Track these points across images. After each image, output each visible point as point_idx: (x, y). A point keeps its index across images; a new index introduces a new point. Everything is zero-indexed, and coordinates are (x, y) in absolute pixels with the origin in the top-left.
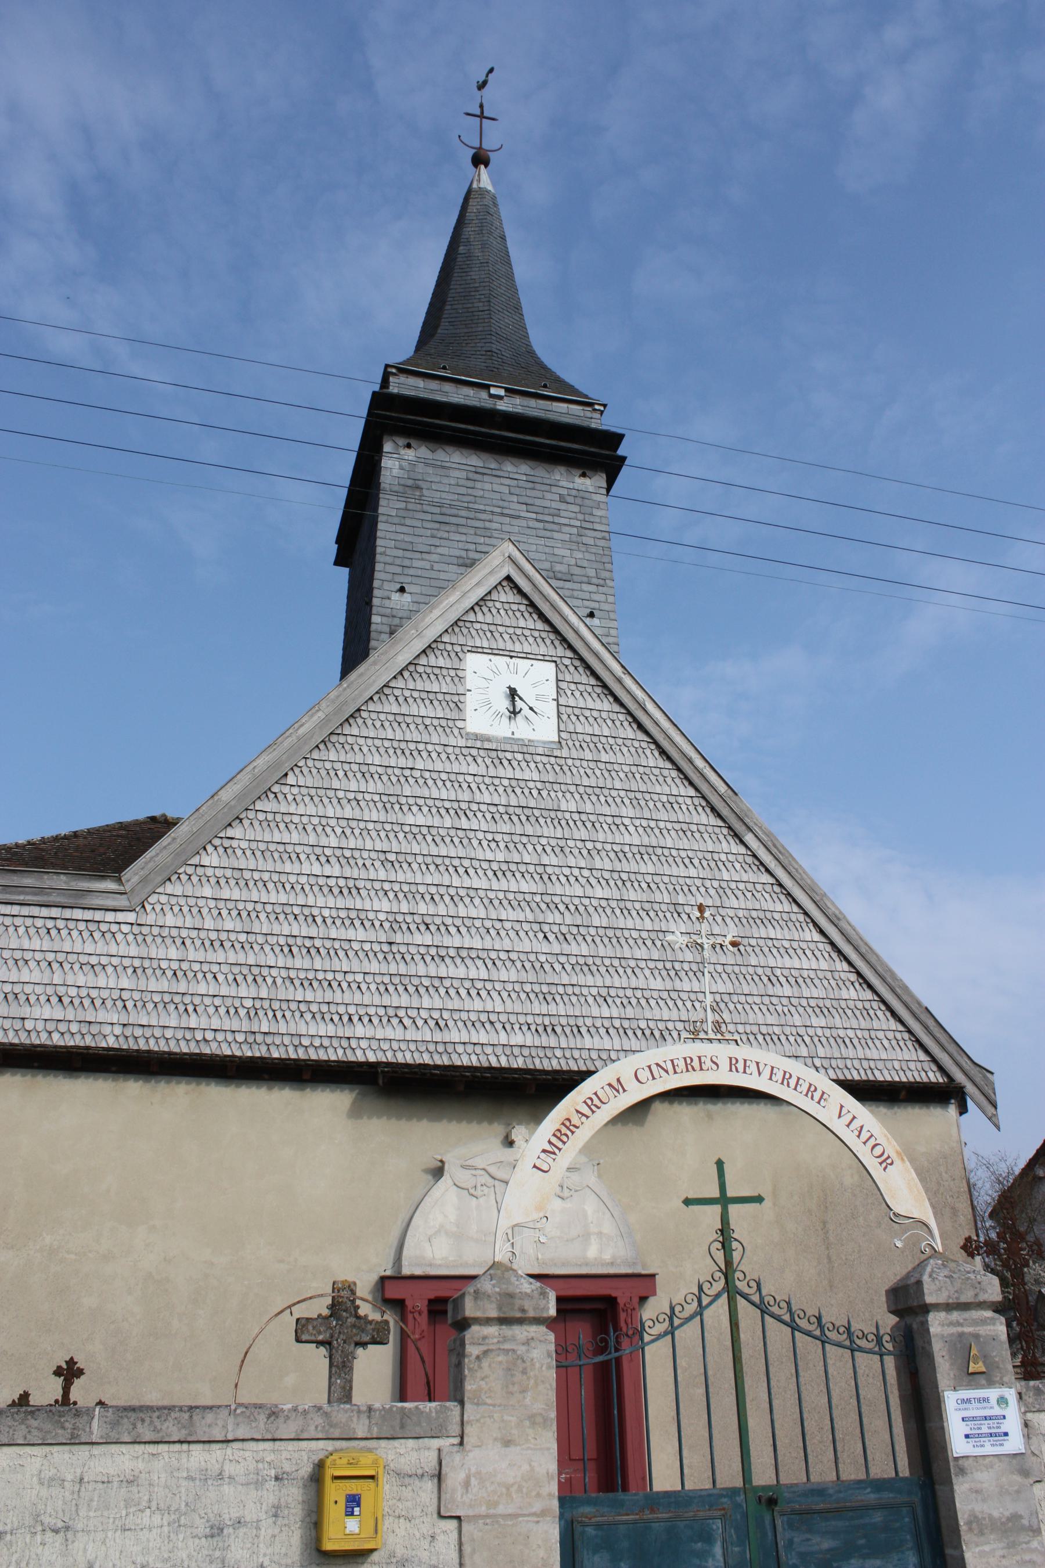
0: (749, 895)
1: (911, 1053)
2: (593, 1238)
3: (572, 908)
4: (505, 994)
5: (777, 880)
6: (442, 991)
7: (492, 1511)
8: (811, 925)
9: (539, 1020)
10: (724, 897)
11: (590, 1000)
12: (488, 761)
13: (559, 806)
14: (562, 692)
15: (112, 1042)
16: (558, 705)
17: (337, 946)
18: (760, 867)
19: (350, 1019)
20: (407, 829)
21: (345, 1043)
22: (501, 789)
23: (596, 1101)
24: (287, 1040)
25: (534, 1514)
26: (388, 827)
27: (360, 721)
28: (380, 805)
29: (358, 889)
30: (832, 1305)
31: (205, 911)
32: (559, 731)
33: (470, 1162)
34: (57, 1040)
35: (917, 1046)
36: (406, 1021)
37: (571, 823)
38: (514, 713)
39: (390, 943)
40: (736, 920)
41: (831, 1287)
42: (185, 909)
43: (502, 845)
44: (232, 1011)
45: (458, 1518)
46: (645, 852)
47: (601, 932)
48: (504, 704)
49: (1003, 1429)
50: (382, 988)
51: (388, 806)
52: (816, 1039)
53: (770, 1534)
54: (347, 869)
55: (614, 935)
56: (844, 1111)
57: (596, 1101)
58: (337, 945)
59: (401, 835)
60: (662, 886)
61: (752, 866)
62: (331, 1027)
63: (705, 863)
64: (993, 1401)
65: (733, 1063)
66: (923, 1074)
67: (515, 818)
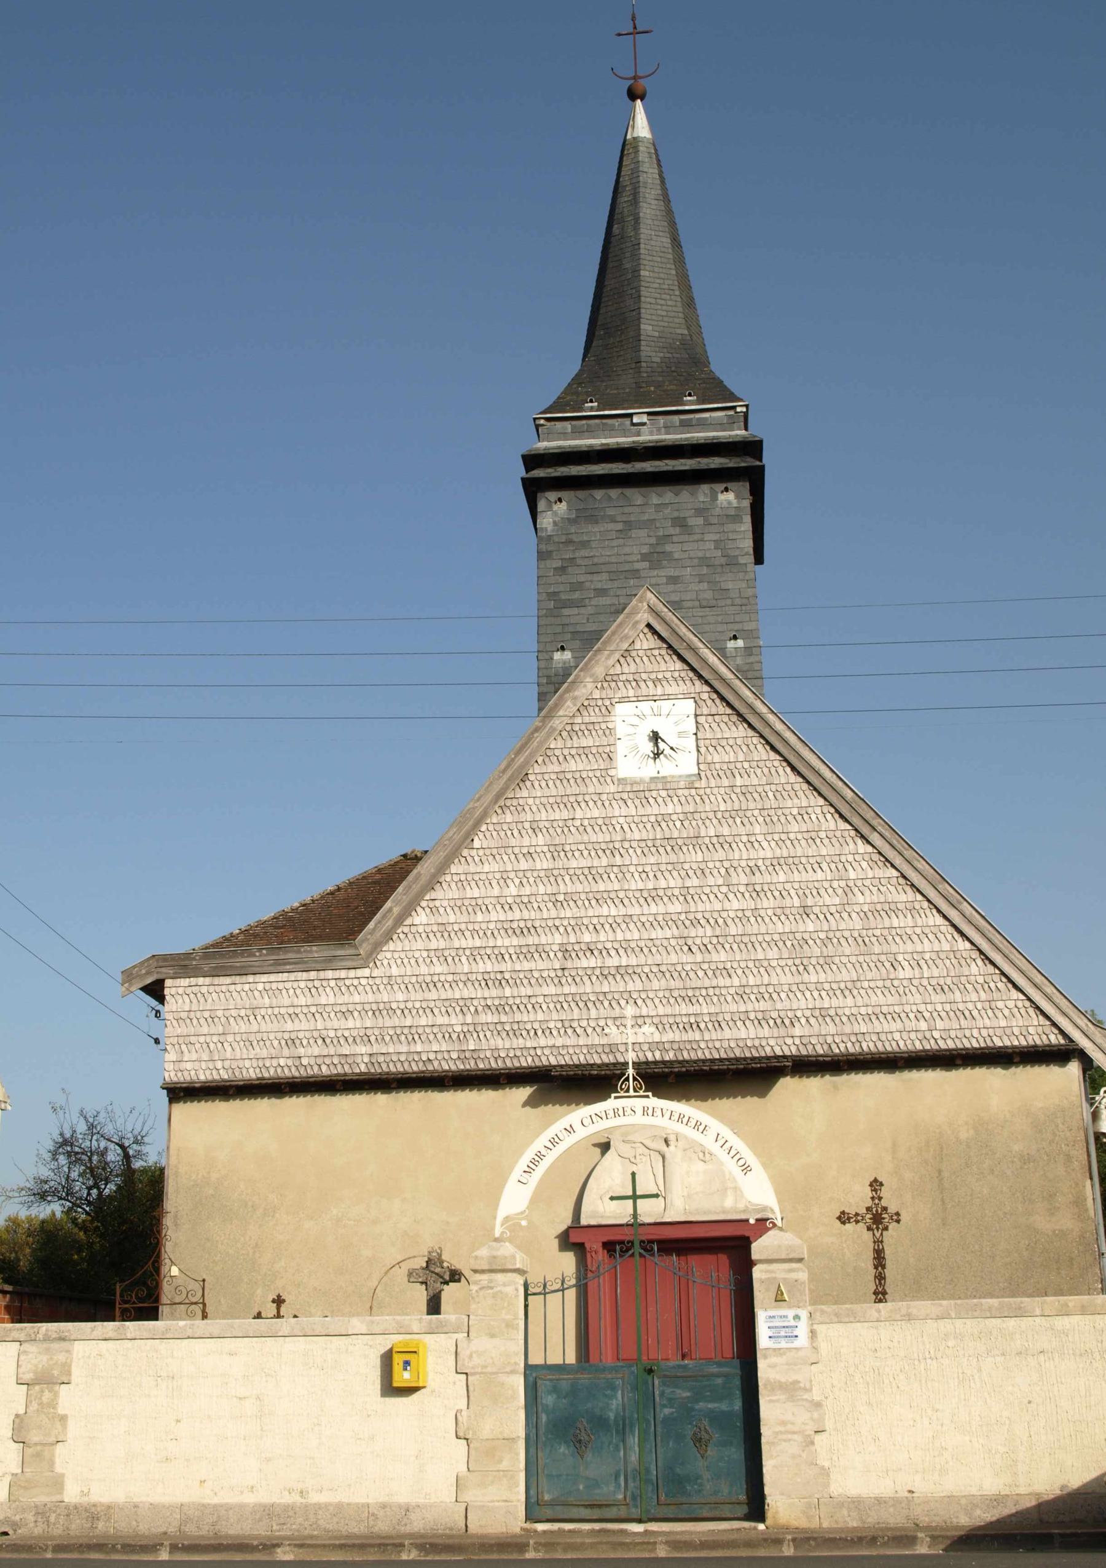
0: (874, 890)
1: (1036, 1019)
2: (729, 1192)
3: (712, 921)
4: (657, 1001)
5: (902, 874)
6: (606, 1003)
7: (484, 1370)
8: (934, 911)
9: (685, 1020)
10: (850, 895)
11: (729, 998)
12: (637, 802)
13: (699, 833)
14: (699, 726)
15: (363, 1068)
16: (697, 739)
17: (521, 976)
18: (887, 864)
19: (536, 1033)
20: (571, 872)
21: (532, 1052)
22: (649, 826)
23: (557, 1140)
24: (488, 1054)
25: (507, 1373)
26: (556, 872)
27: (528, 783)
28: (549, 855)
29: (535, 928)
30: (944, 1239)
31: (420, 960)
32: (698, 764)
33: (629, 1138)
34: (325, 1070)
35: (1038, 1013)
36: (578, 1030)
37: (711, 847)
38: (657, 755)
39: (563, 969)
40: (862, 914)
41: (944, 1224)
42: (406, 961)
43: (651, 875)
44: (447, 1036)
45: (466, 1374)
46: (776, 863)
47: (738, 939)
48: (649, 747)
49: (795, 1333)
50: (558, 1007)
51: (556, 854)
52: (935, 1014)
53: (651, 1388)
54: (525, 912)
55: (745, 942)
56: (720, 1137)
57: (557, 1140)
58: (521, 975)
59: (567, 878)
60: (793, 892)
61: (879, 862)
62: (521, 1040)
63: (833, 866)
64: (791, 1317)
65: (645, 1111)
66: (1044, 1037)
67: (662, 850)
